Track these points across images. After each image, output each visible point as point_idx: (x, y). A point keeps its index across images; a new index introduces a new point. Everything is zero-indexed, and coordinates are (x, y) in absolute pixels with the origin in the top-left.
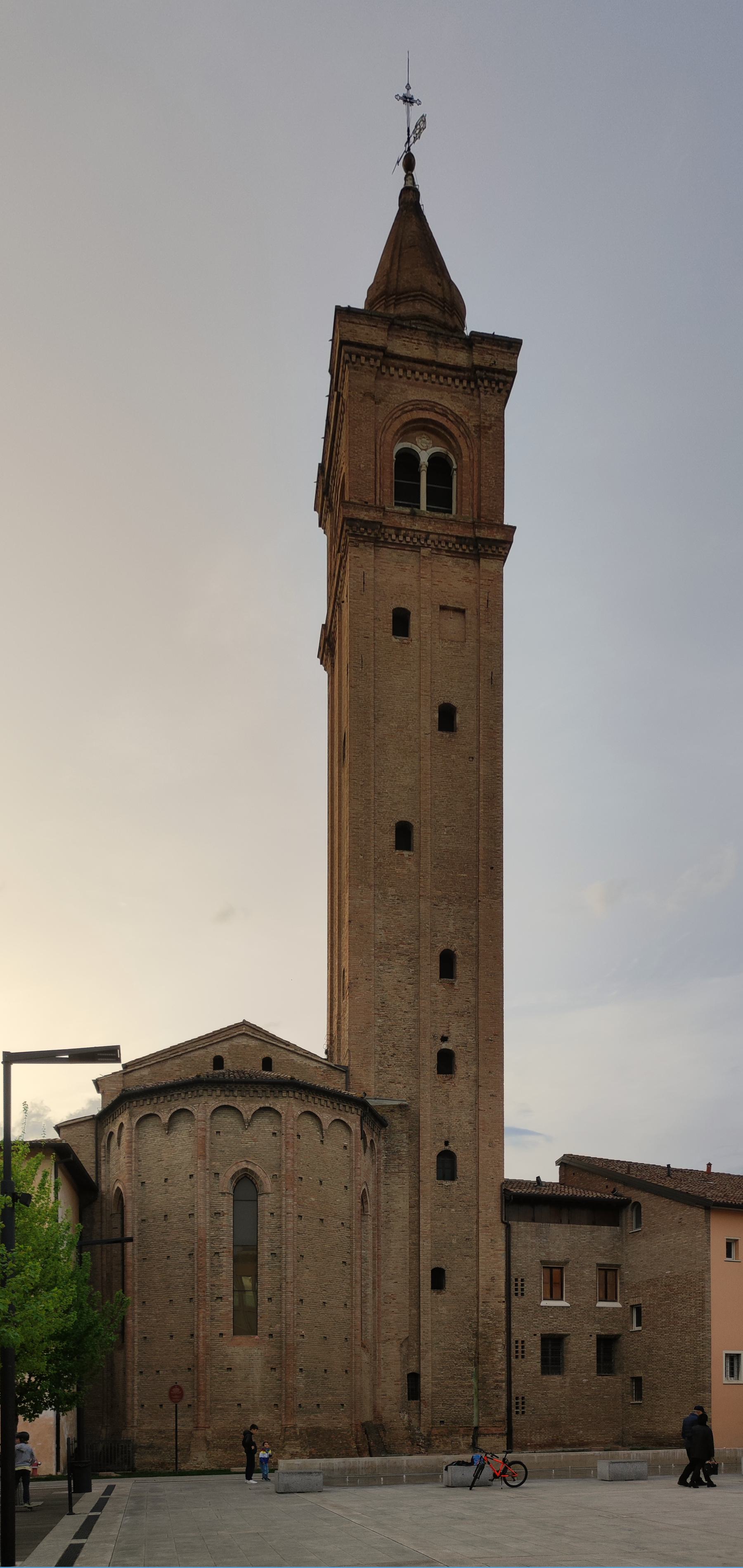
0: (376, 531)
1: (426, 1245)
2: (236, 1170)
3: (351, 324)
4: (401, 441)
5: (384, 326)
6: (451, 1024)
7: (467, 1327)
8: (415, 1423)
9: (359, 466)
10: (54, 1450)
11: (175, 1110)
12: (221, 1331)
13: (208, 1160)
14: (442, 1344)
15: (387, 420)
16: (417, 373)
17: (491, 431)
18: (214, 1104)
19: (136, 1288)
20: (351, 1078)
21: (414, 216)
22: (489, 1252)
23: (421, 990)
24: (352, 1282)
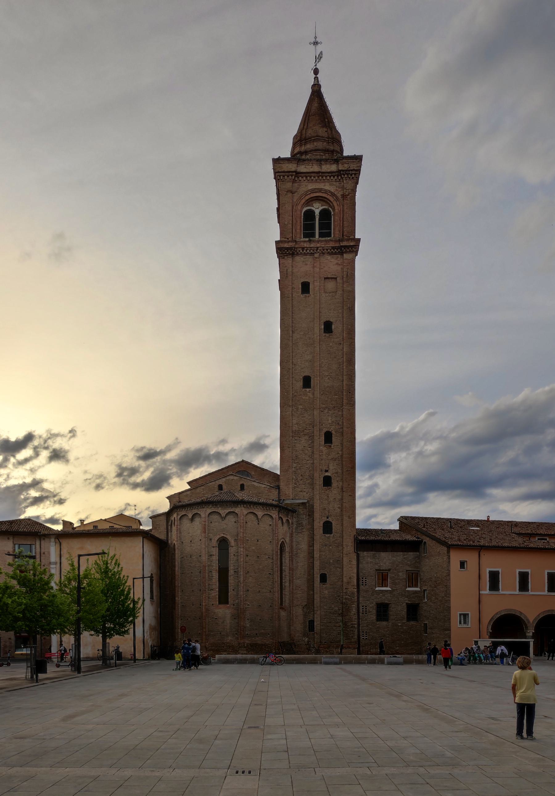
0: (292, 251)
1: (317, 564)
2: (219, 537)
3: (280, 164)
4: (306, 207)
5: (296, 162)
7: (338, 600)
10: (142, 650)
12: (213, 603)
13: (207, 534)
16: (312, 177)
17: (349, 196)
18: (209, 511)
19: (179, 585)
20: (281, 491)
21: (316, 99)
23: (315, 450)
24: (273, 582)
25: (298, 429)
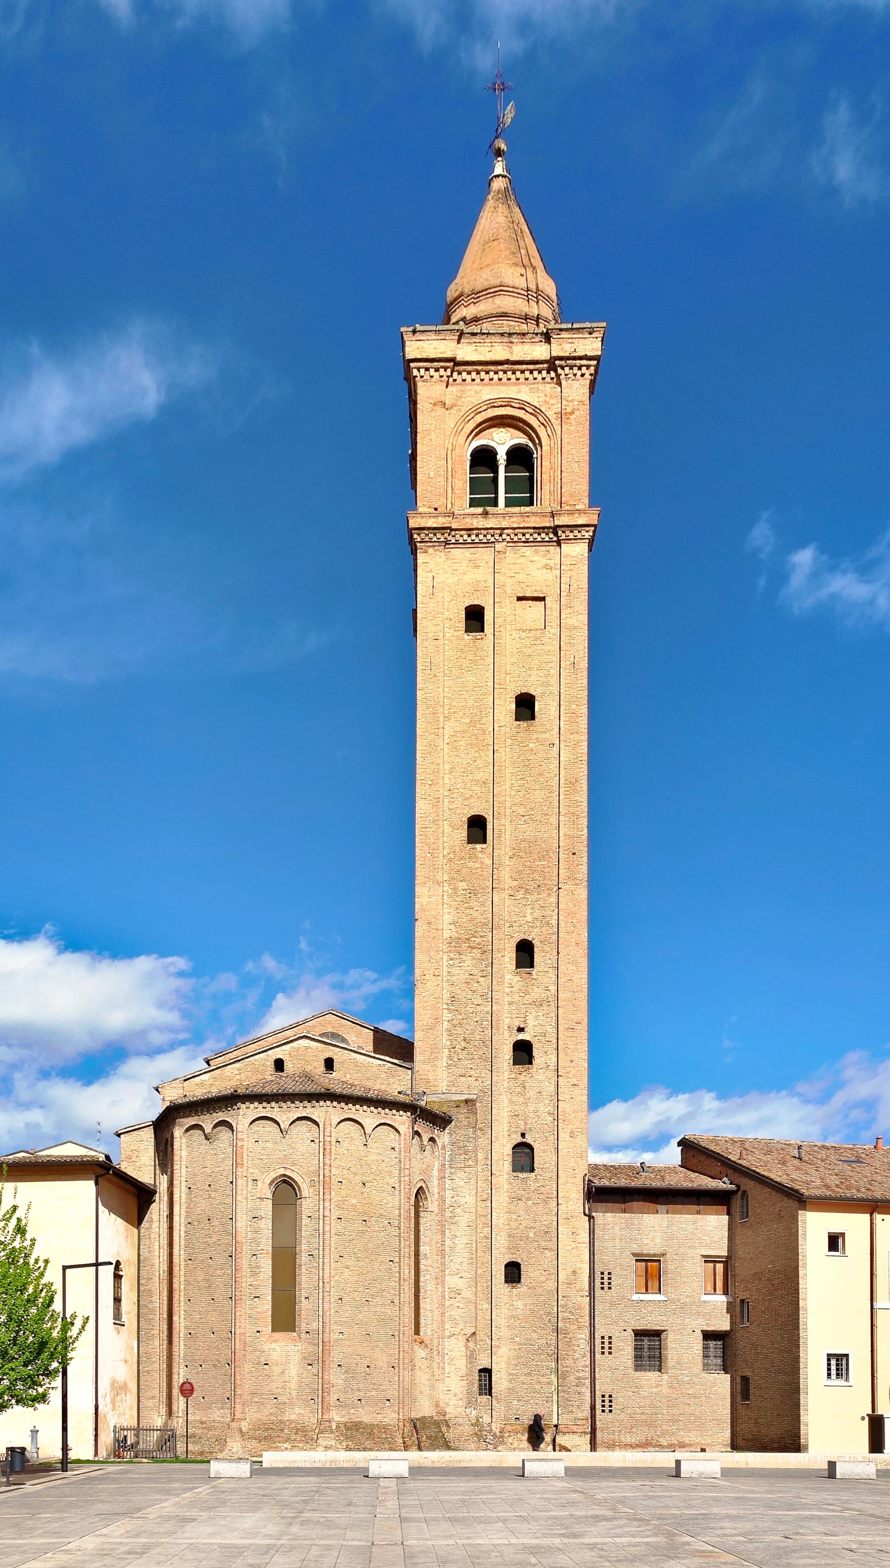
2: (274, 1176)
6: (527, 1014)
8: (486, 1419)
9: (429, 474)
11: (217, 1121)
14: (517, 1339)
15: (459, 423)
22: (570, 1245)
25: (456, 935)
